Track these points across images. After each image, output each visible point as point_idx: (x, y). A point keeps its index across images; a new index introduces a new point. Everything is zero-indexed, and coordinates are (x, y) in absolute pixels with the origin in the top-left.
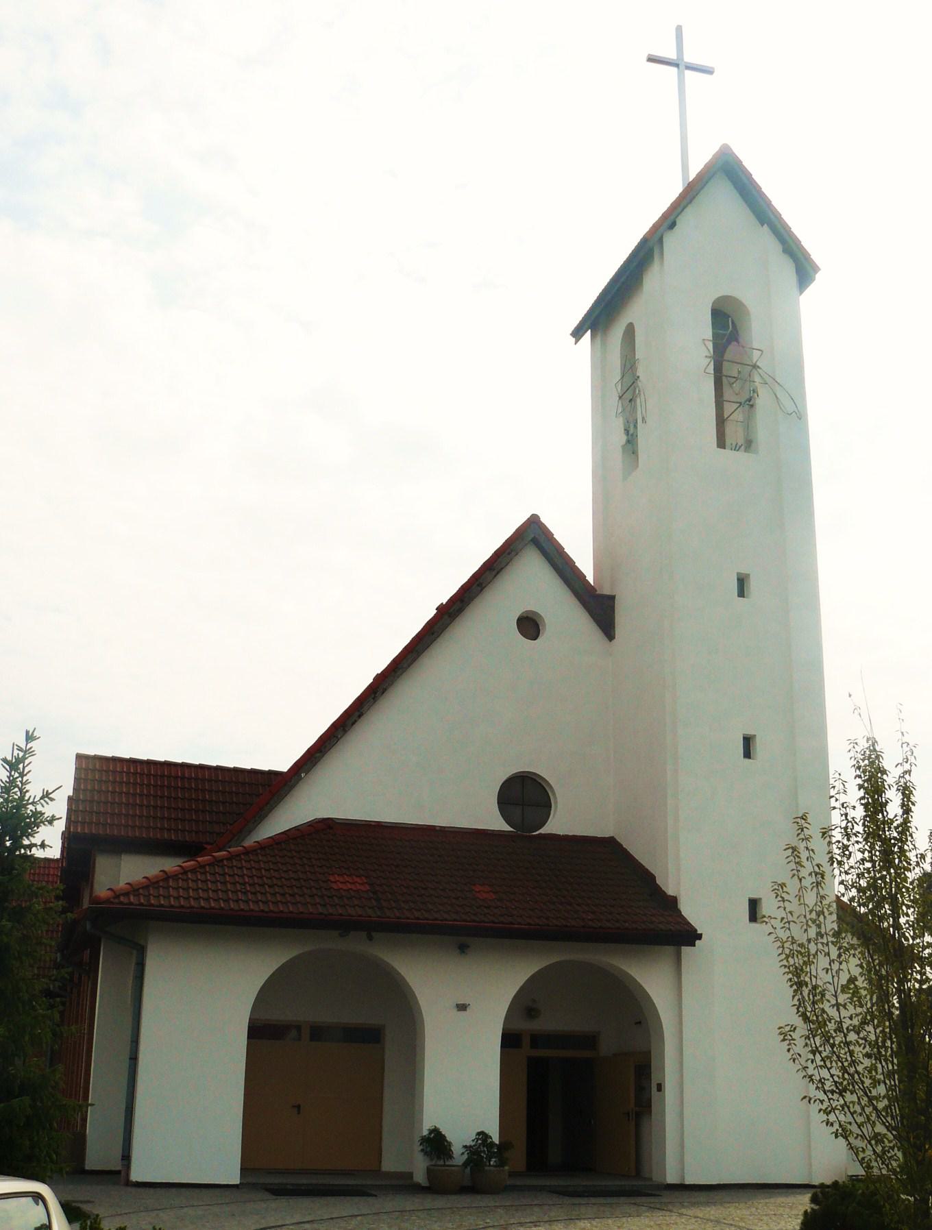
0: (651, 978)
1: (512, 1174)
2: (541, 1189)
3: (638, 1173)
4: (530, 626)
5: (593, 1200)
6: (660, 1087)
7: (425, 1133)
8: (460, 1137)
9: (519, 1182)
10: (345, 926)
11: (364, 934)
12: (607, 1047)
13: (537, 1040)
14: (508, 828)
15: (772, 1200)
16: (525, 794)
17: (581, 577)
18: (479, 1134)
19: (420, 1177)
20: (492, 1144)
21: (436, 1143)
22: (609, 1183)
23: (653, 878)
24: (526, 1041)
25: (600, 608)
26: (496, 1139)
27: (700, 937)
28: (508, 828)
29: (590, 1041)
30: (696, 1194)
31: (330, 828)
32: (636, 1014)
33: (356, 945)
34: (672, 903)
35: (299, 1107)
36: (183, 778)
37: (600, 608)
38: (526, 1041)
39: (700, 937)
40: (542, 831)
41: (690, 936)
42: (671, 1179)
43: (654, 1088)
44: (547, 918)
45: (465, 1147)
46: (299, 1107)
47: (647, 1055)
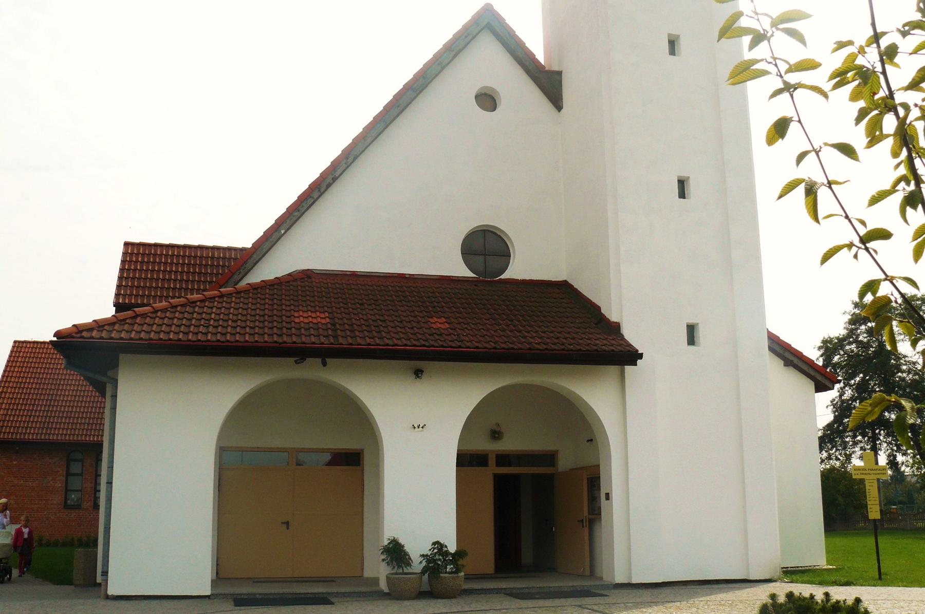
0: (596, 394)
1: (468, 578)
2: (498, 591)
3: (592, 573)
4: (487, 100)
5: (541, 603)
6: (608, 496)
7: (386, 543)
8: (417, 548)
9: (477, 586)
10: (300, 353)
11: (319, 360)
12: (564, 463)
13: (503, 459)
14: (469, 274)
15: (713, 597)
16: (486, 246)
17: (531, 56)
18: (434, 544)
19: (383, 586)
20: (447, 553)
21: (395, 552)
22: (561, 584)
23: (598, 308)
24: (492, 461)
25: (550, 84)
26: (452, 548)
27: (640, 356)
28: (469, 274)
29: (549, 458)
30: (721, 591)
31: (309, 277)
32: (582, 426)
33: (311, 371)
34: (615, 329)
35: (287, 523)
36: (213, 258)
37: (550, 84)
38: (492, 461)
39: (640, 356)
40: (502, 277)
41: (632, 356)
42: (619, 579)
43: (603, 497)
44: (495, 343)
45: (423, 556)
46: (287, 523)
47: (597, 467)
